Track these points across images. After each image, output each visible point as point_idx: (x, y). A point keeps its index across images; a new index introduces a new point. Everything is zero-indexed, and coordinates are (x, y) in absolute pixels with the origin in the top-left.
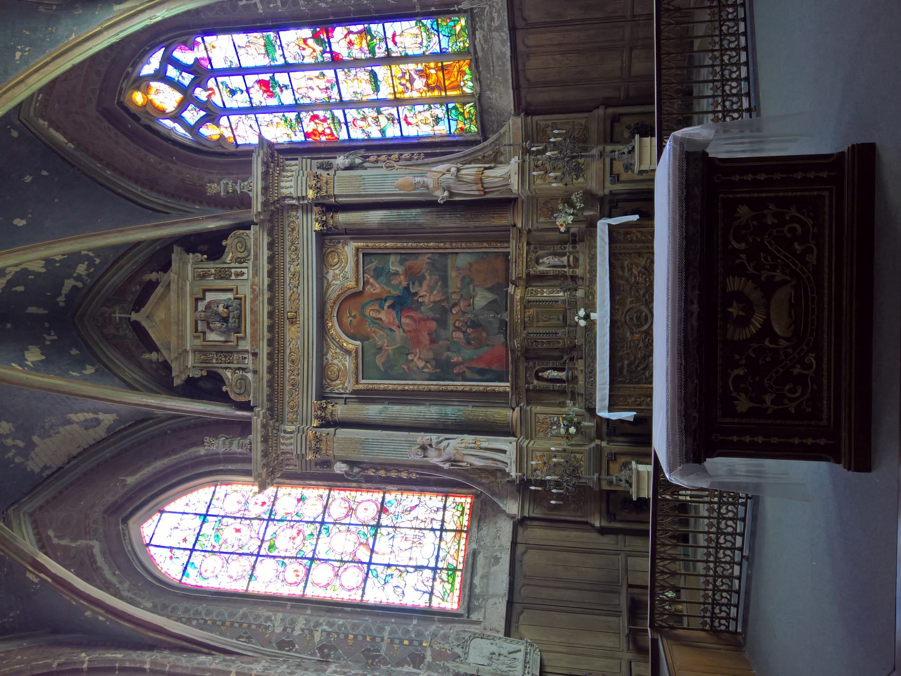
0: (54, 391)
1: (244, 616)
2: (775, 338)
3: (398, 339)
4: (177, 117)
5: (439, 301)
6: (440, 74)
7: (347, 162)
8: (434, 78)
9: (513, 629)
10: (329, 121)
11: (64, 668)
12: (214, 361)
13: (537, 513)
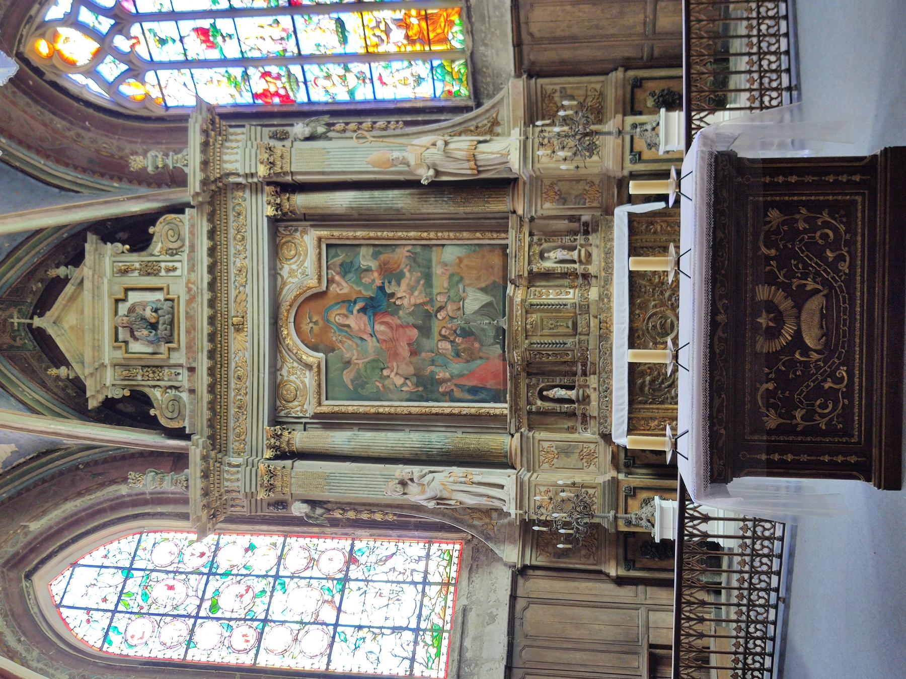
2: (806, 350)
4: (91, 71)
5: (421, 304)
6: (424, 24)
7: (307, 131)
12: (139, 378)
13: (541, 561)
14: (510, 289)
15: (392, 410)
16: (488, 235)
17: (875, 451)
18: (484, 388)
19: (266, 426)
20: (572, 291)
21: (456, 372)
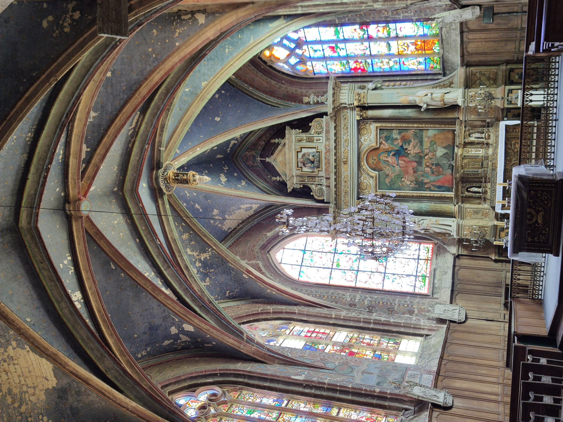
0: (239, 197)
1: (332, 293)
2: (539, 224)
3: (397, 171)
4: (287, 62)
5: (418, 153)
6: (423, 44)
7: (374, 87)
8: (419, 46)
9: (453, 301)
10: (363, 63)
11: (263, 312)
12: (306, 181)
13: (465, 253)
14: (456, 149)
15: (406, 194)
16: (447, 126)
17: (553, 248)
18: (444, 186)
19: (356, 200)
20: (481, 150)
21: (432, 180)
